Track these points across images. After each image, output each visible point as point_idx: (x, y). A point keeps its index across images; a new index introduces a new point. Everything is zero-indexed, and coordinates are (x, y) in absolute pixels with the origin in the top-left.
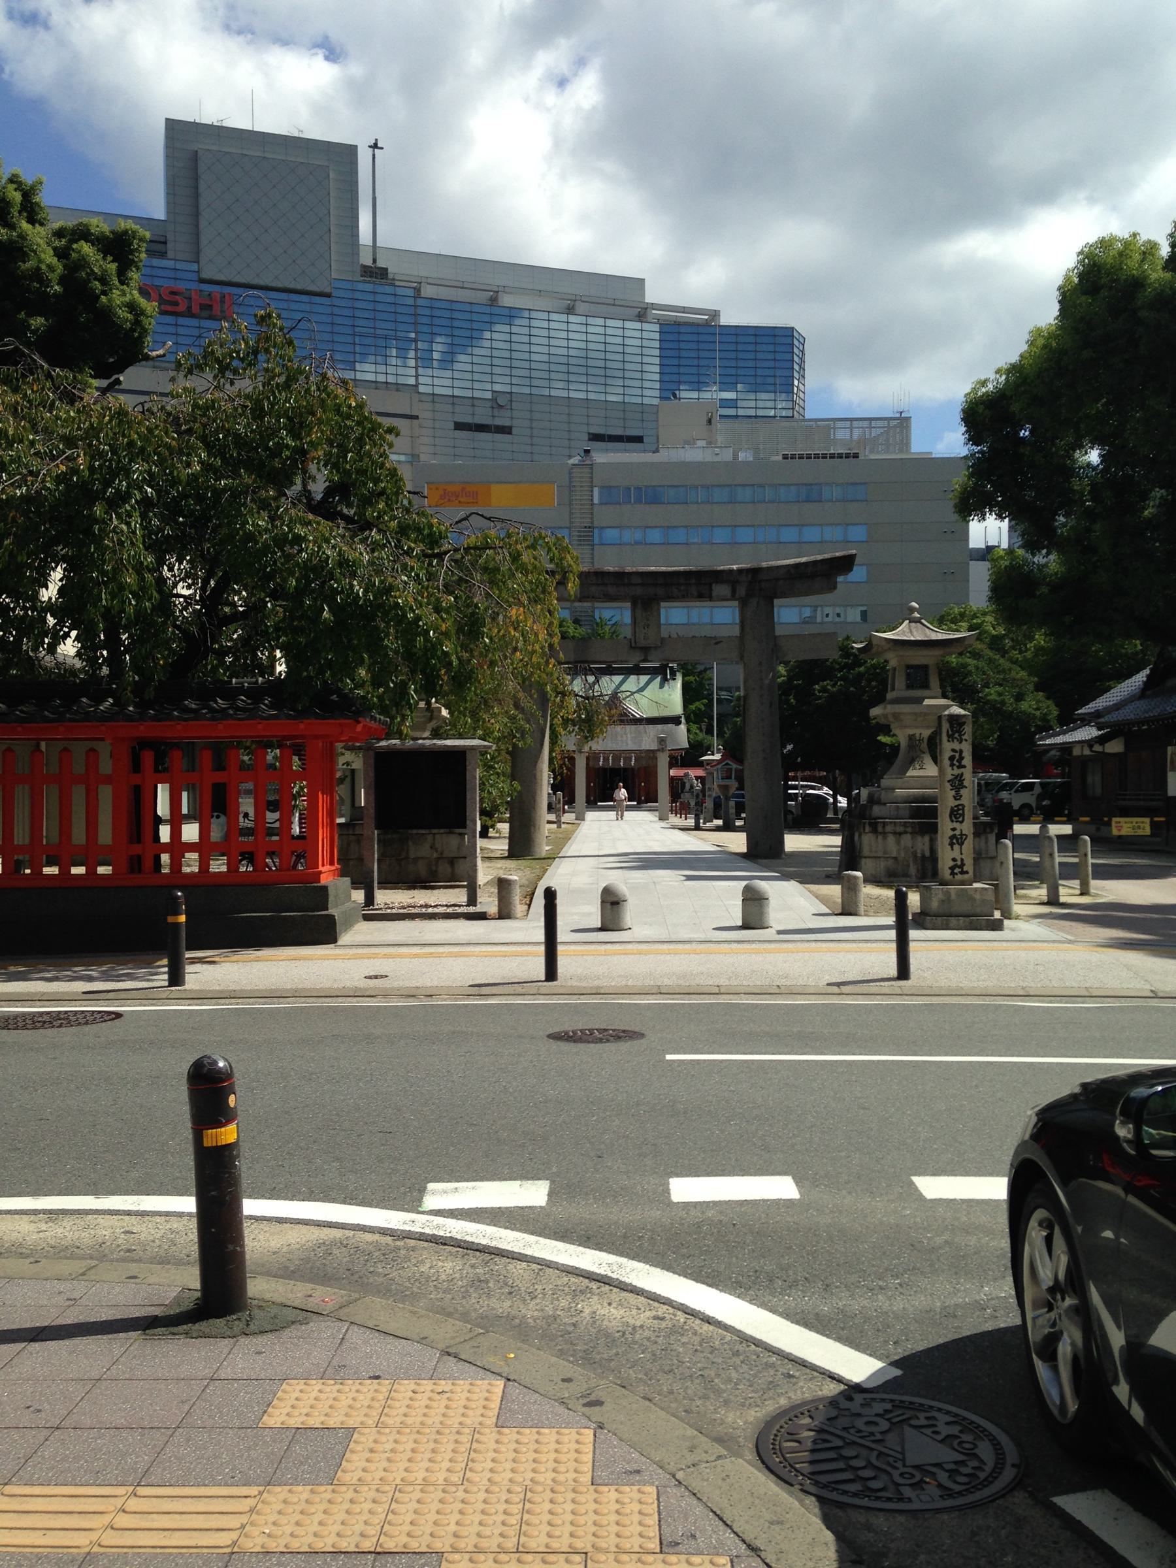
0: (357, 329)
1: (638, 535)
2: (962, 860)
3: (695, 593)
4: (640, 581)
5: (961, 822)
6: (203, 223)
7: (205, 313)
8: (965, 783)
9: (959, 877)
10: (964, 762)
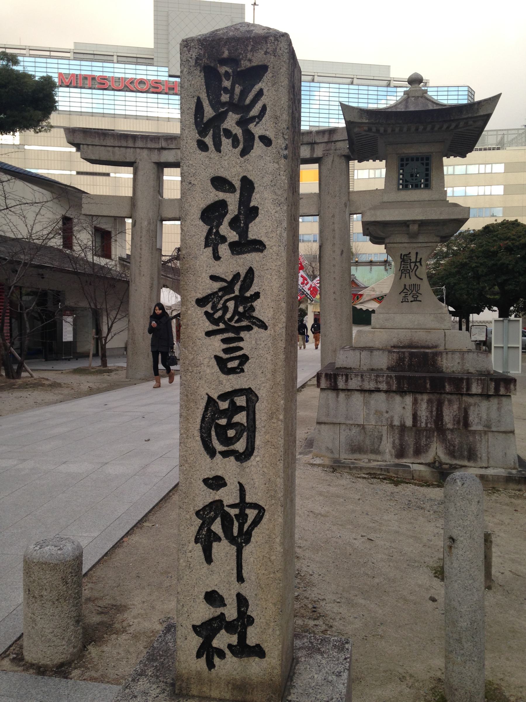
5: (244, 457)
7: (172, 92)
8: (263, 309)
10: (256, 230)
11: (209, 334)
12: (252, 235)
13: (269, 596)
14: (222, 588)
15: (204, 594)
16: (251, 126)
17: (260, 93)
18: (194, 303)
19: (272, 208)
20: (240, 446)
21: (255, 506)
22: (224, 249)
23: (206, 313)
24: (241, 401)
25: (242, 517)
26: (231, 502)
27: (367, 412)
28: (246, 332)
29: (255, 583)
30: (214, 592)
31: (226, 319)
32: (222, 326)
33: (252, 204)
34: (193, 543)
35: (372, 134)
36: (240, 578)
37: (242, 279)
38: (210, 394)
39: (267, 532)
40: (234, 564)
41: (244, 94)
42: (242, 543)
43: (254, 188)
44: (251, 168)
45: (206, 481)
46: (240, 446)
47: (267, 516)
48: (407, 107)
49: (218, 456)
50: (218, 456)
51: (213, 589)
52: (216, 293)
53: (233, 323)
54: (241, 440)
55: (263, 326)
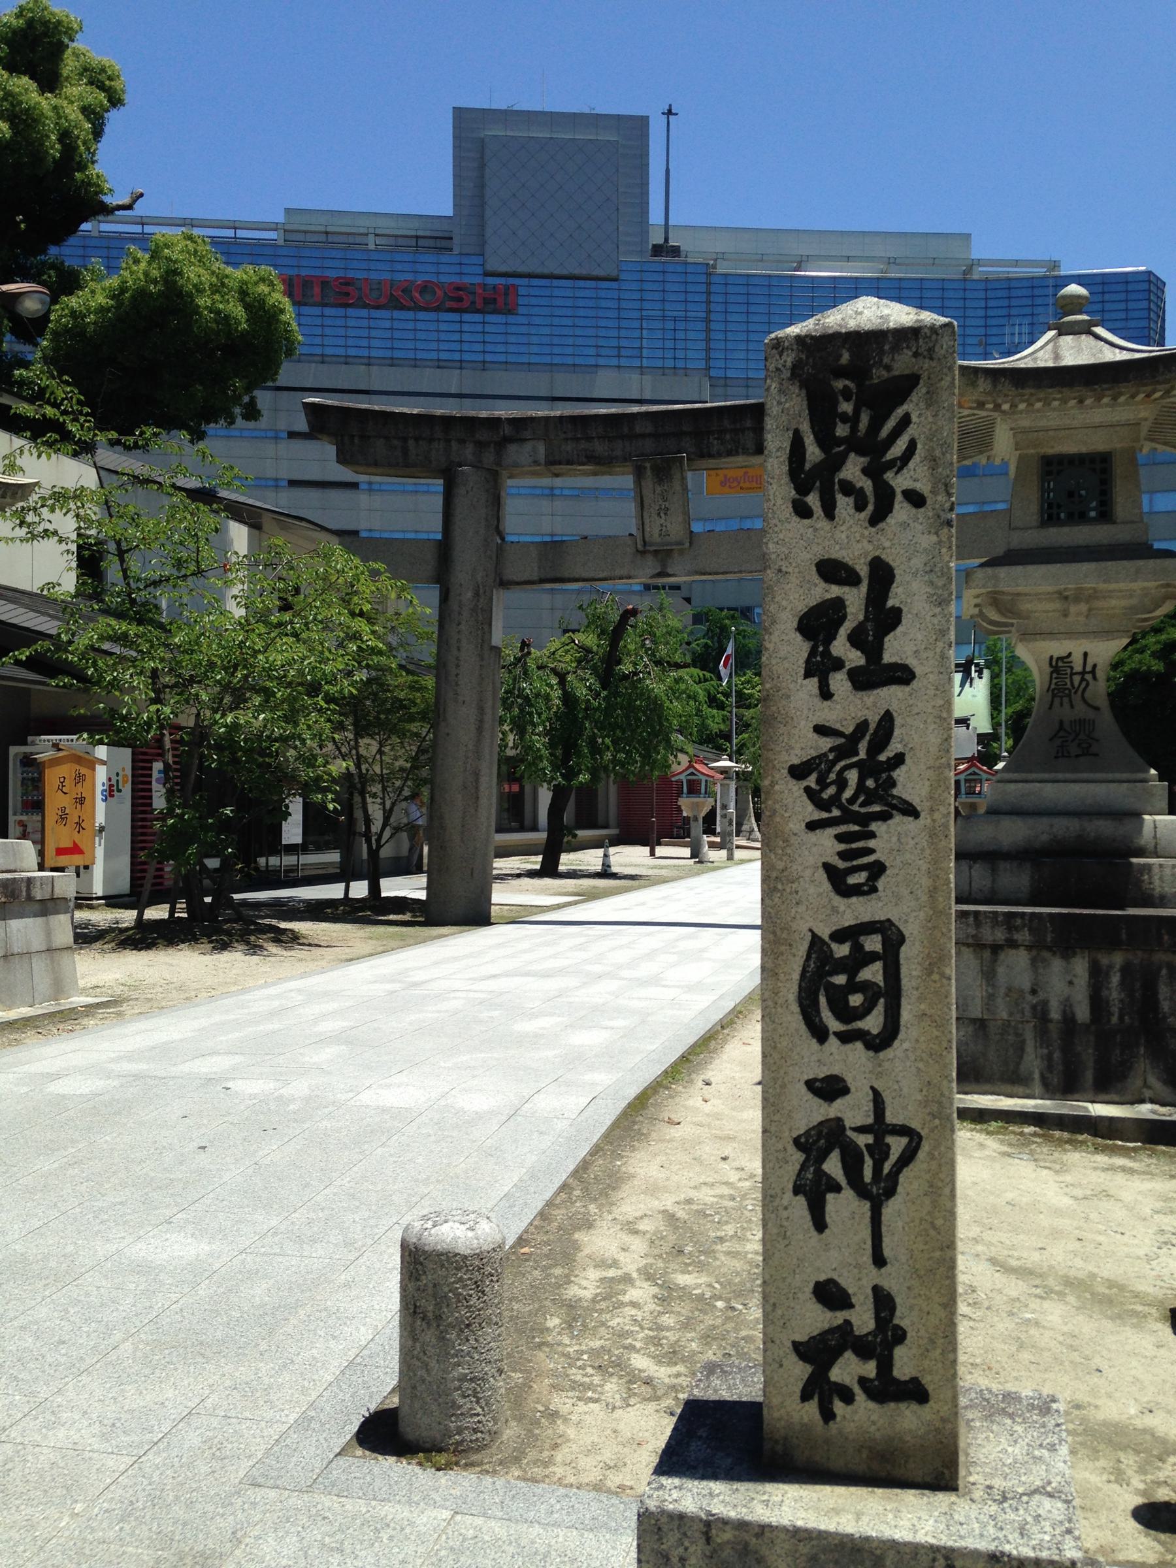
0: (644, 313)
2: (883, 1301)
4: (649, 429)
5: (880, 1043)
6: (488, 213)
8: (910, 783)
9: (862, 1417)
10: (896, 648)
11: (812, 826)
12: (888, 657)
13: (934, 1290)
14: (845, 1274)
15: (812, 1285)
16: (889, 476)
17: (906, 421)
18: (785, 772)
19: (927, 608)
20: (873, 1023)
21: (903, 1130)
22: (839, 682)
23: (808, 790)
24: (873, 943)
25: (879, 1151)
26: (859, 1122)
27: (990, 991)
28: (879, 823)
29: (906, 1267)
30: (831, 1282)
31: (844, 801)
32: (836, 812)
33: (890, 603)
34: (789, 1194)
35: (983, 413)
36: (879, 1260)
37: (871, 731)
38: (816, 930)
39: (927, 1177)
40: (866, 1233)
41: (876, 424)
42: (879, 1195)
43: (893, 576)
44: (887, 544)
45: (810, 1085)
46: (873, 1023)
47: (925, 1147)
48: (1057, 357)
49: (833, 1041)
50: (833, 1041)
51: (829, 1276)
52: (825, 755)
53: (855, 808)
54: (875, 1012)
55: (911, 811)
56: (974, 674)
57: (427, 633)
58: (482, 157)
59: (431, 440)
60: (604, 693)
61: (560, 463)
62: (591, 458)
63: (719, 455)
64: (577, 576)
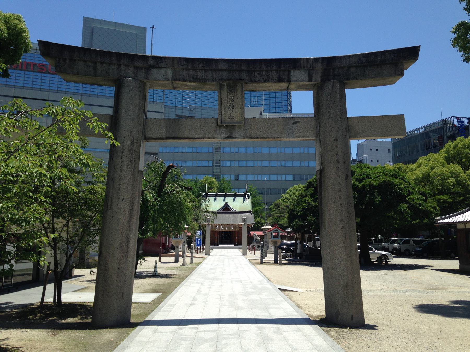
1: (236, 150)
3: (275, 78)
4: (226, 67)
56: (247, 198)
57: (98, 165)
58: (92, 33)
59: (110, 64)
60: (159, 199)
61: (179, 80)
62: (195, 79)
63: (260, 82)
64: (186, 136)
